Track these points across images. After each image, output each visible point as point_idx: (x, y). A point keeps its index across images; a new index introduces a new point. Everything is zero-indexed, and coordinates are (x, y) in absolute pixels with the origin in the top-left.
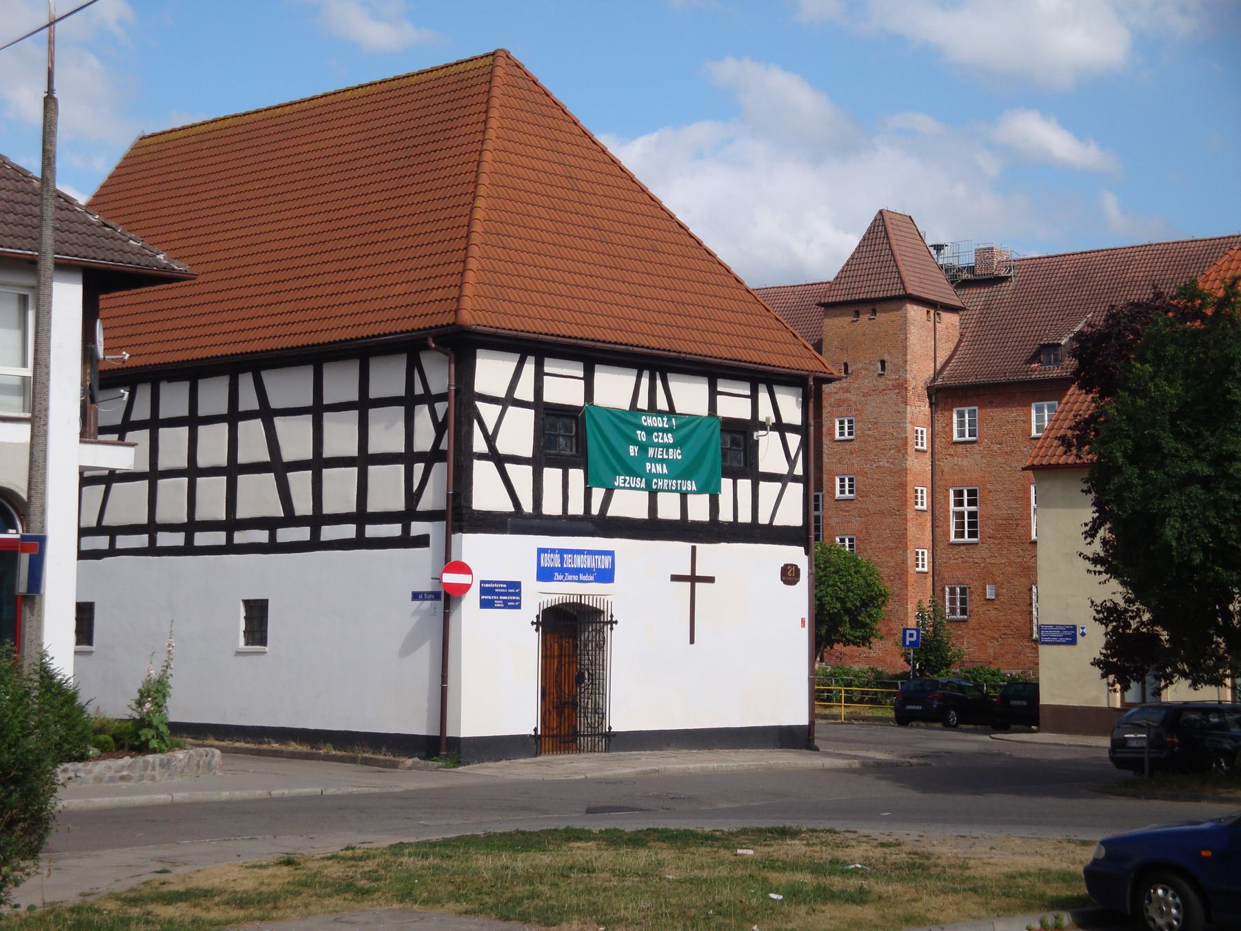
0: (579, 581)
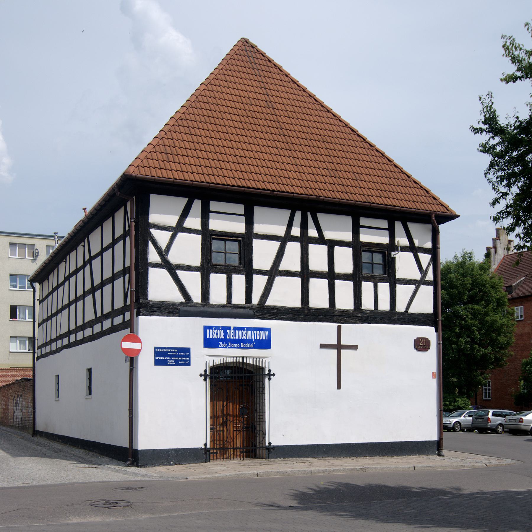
0: (240, 348)
